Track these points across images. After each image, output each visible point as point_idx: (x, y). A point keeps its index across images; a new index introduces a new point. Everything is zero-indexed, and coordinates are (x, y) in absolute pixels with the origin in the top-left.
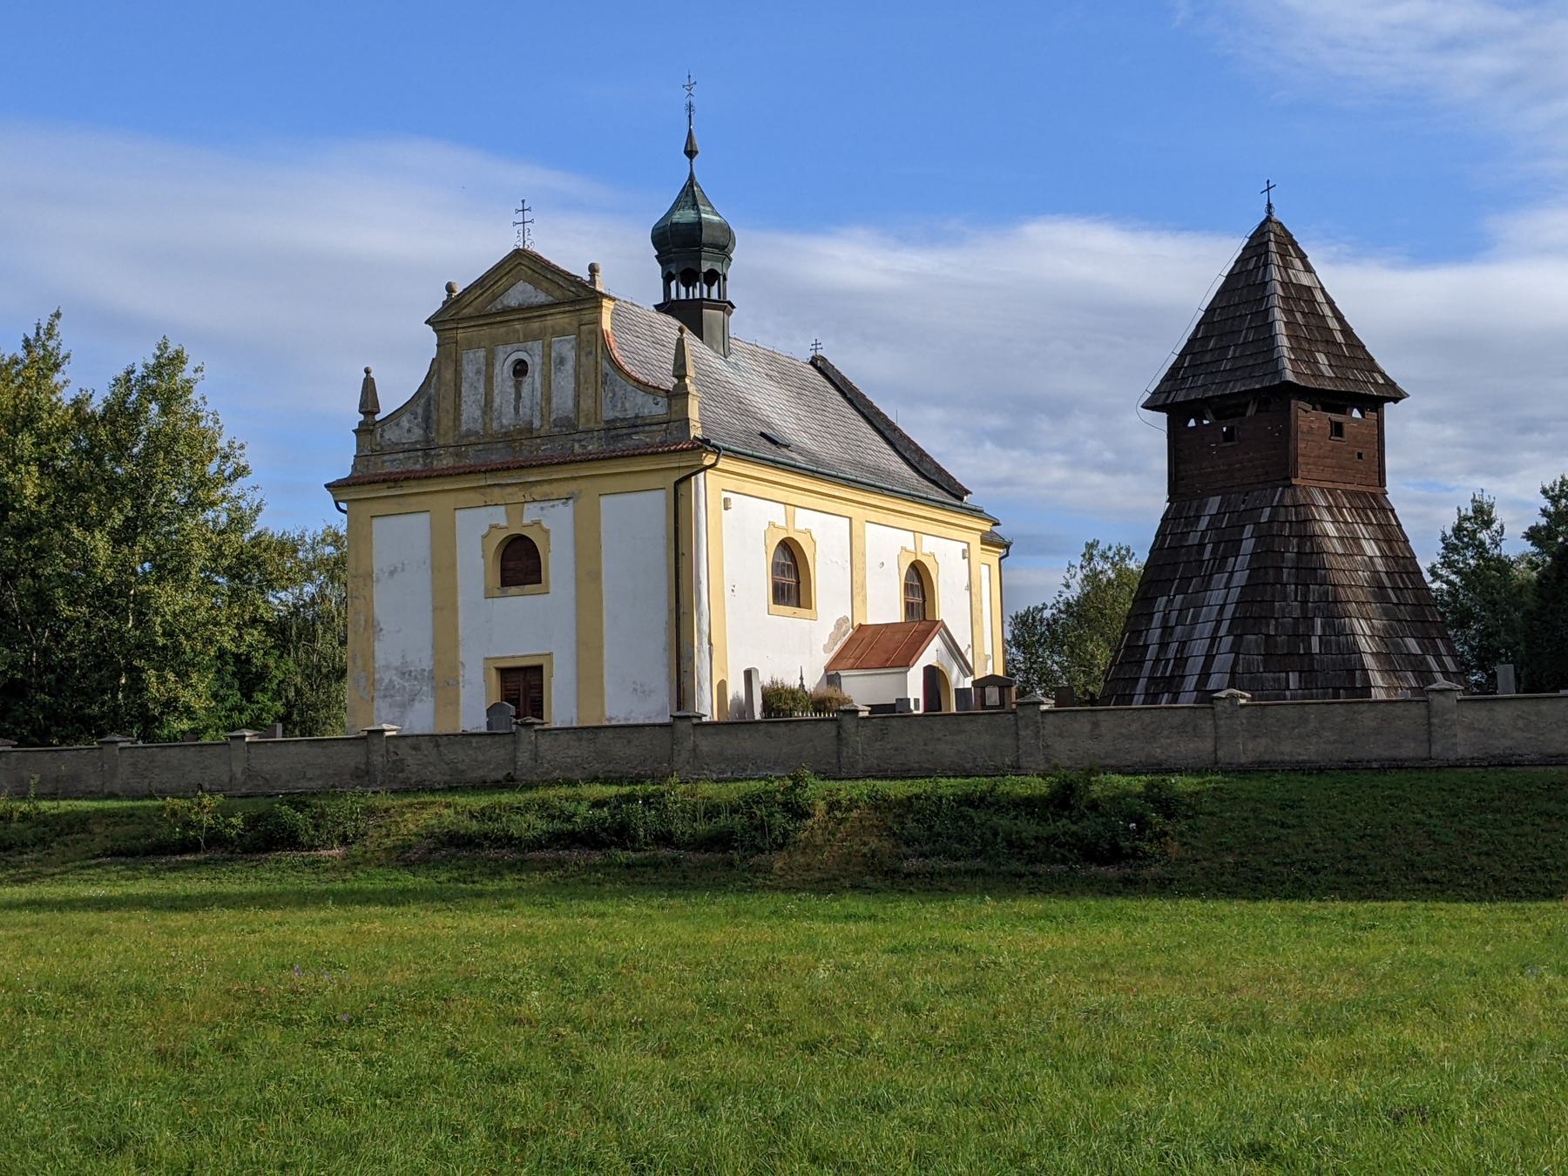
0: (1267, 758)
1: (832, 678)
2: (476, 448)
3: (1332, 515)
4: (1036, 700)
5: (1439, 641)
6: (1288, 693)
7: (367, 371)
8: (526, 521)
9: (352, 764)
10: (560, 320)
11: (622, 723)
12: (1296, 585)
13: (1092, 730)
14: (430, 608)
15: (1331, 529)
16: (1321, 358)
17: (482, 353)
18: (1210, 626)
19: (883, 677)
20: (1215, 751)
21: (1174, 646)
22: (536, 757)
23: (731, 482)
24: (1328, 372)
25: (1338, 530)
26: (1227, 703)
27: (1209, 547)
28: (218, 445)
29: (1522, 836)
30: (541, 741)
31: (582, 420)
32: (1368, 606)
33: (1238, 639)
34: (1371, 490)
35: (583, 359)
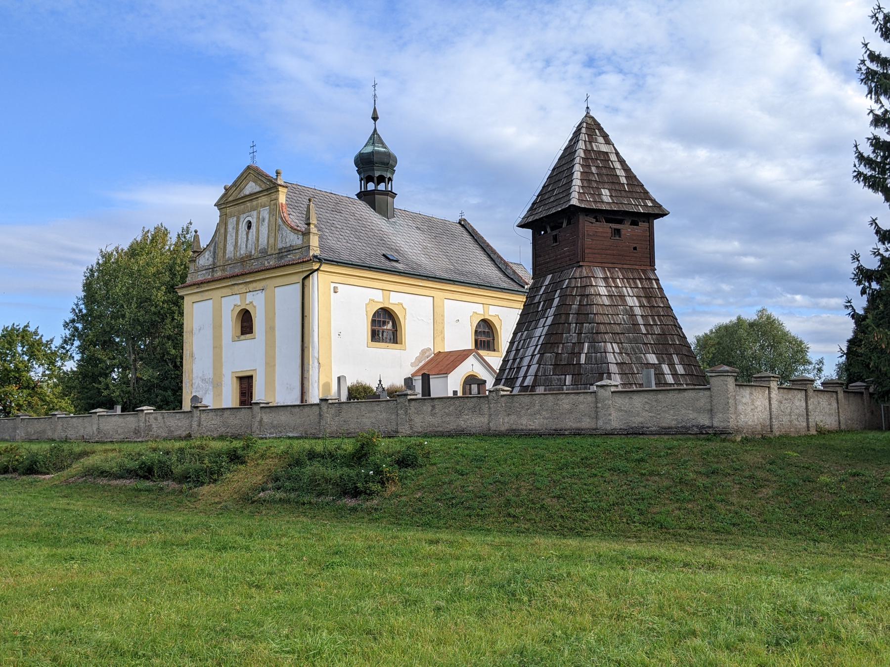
0: (514, 427)
2: (230, 266)
6: (565, 387)
8: (247, 302)
9: (134, 427)
10: (264, 200)
11: (282, 404)
12: (576, 323)
13: (432, 411)
15: (603, 291)
16: (605, 192)
17: (235, 219)
19: (439, 379)
20: (489, 424)
25: (608, 291)
27: (542, 303)
31: (269, 249)
35: (271, 218)
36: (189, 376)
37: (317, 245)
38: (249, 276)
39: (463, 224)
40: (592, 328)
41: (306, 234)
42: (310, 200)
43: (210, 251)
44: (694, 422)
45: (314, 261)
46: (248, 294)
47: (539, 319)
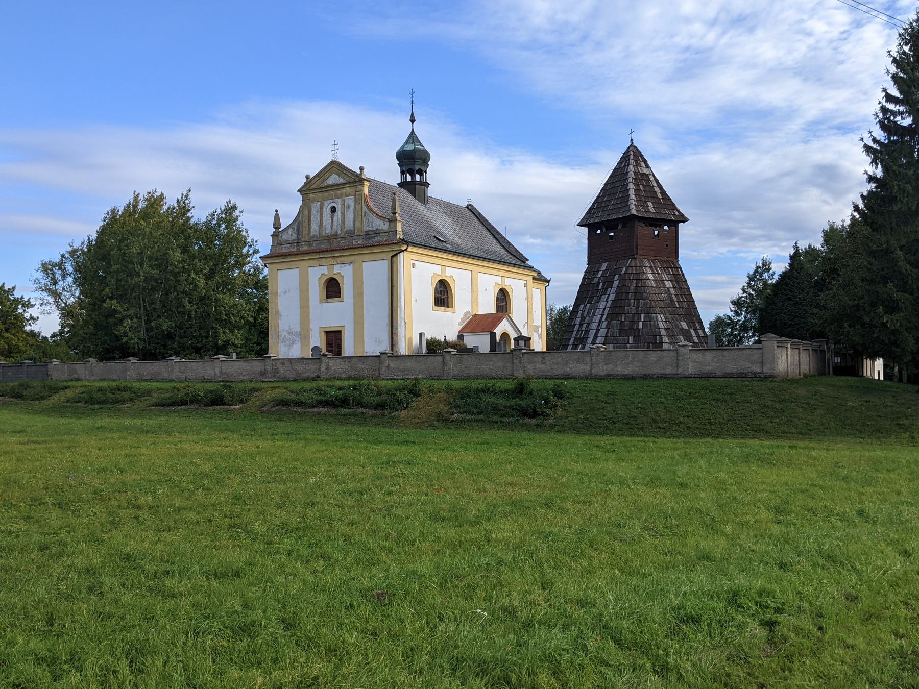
0: (611, 373)
1: (460, 337)
3: (652, 270)
4: (520, 348)
5: (697, 324)
6: (628, 345)
7: (276, 211)
8: (335, 272)
9: (259, 370)
10: (348, 190)
11: (371, 354)
12: (634, 300)
13: (542, 361)
14: (299, 307)
15: (651, 276)
16: (650, 204)
17: (319, 203)
18: (599, 317)
20: (591, 370)
21: (585, 325)
22: (328, 368)
23: (415, 257)
24: (652, 210)
25: (654, 277)
26: (596, 350)
27: (601, 284)
28: (248, 241)
29: (704, 409)
30: (330, 362)
31: (356, 231)
32: (665, 309)
33: (609, 322)
34: (672, 260)
35: (357, 206)
36: (275, 329)
37: (401, 230)
38: (338, 251)
39: (470, 208)
40: (647, 303)
41: (393, 221)
42: (394, 194)
43: (293, 228)
44: (749, 370)
45: (403, 244)
46: (335, 266)
47: (601, 296)
